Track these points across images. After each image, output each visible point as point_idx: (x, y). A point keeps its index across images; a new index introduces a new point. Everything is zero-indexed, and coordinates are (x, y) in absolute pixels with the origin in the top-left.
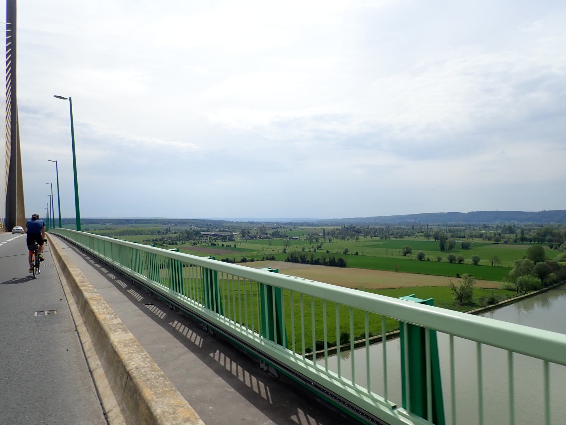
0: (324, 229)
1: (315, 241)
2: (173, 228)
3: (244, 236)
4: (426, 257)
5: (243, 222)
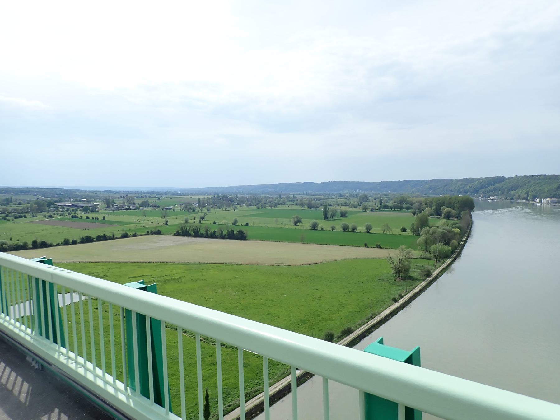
0: (199, 198)
1: (192, 211)
2: (346, 192)
3: (108, 207)
4: (320, 226)
5: (98, 191)
